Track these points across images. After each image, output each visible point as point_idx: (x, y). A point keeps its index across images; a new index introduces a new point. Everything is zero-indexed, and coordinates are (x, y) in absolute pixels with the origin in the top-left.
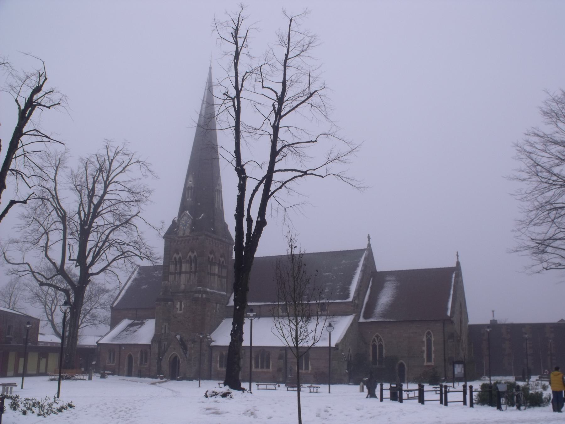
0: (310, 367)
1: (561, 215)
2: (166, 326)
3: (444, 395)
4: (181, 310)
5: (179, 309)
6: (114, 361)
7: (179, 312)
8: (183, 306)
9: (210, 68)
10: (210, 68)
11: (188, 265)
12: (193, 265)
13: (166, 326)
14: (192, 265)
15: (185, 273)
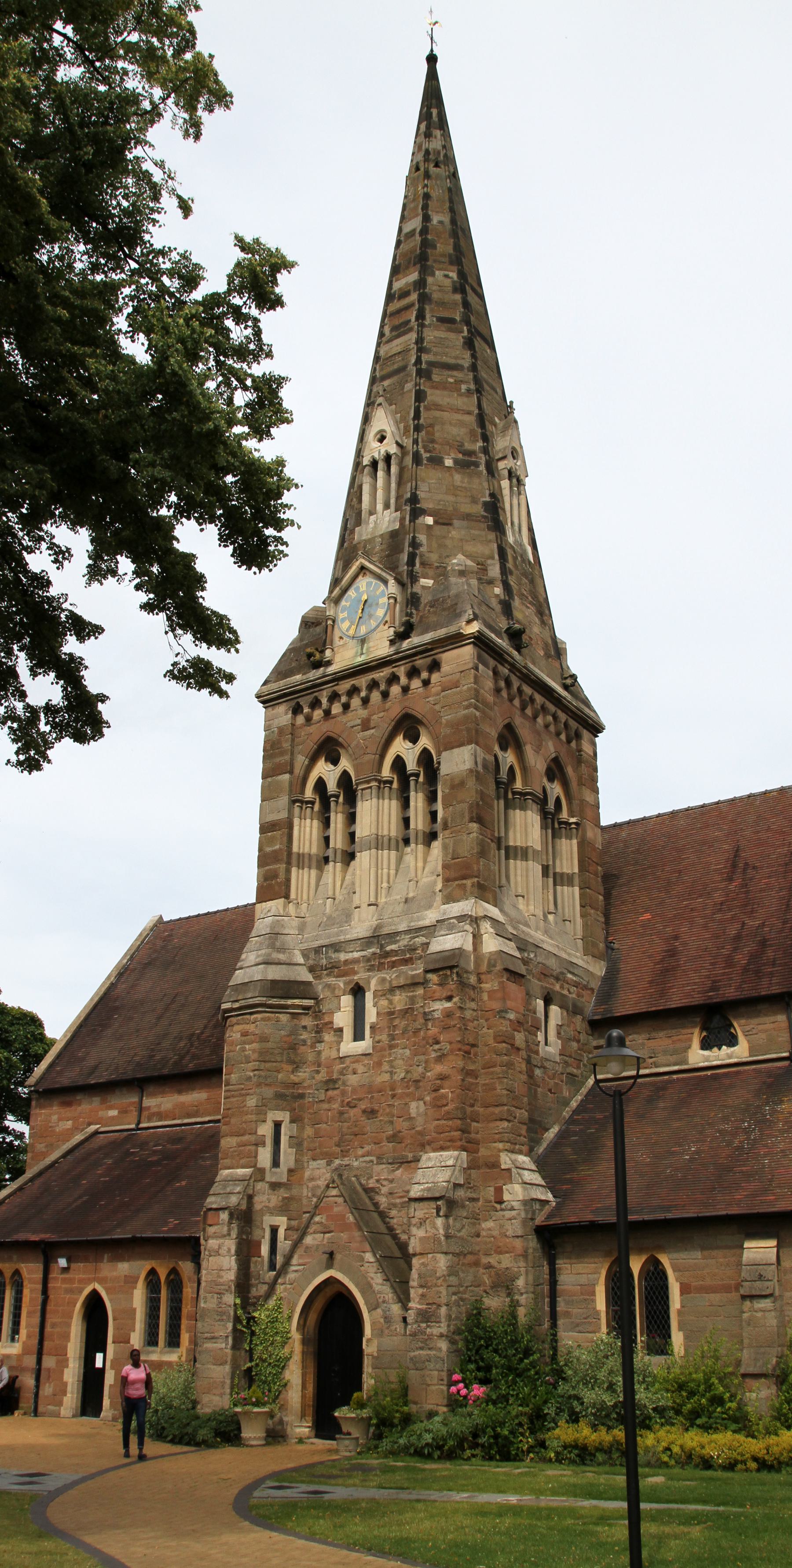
0: (677, 1338)
1: (525, 1189)
2: (277, 1125)
3: (164, 1294)
4: (358, 1035)
5: (348, 1033)
6: (15, 1331)
7: (349, 1047)
8: (371, 1015)
9: (432, 59)
10: (432, 59)
11: (391, 807)
12: (417, 800)
13: (277, 1125)
14: (412, 803)
15: (378, 843)
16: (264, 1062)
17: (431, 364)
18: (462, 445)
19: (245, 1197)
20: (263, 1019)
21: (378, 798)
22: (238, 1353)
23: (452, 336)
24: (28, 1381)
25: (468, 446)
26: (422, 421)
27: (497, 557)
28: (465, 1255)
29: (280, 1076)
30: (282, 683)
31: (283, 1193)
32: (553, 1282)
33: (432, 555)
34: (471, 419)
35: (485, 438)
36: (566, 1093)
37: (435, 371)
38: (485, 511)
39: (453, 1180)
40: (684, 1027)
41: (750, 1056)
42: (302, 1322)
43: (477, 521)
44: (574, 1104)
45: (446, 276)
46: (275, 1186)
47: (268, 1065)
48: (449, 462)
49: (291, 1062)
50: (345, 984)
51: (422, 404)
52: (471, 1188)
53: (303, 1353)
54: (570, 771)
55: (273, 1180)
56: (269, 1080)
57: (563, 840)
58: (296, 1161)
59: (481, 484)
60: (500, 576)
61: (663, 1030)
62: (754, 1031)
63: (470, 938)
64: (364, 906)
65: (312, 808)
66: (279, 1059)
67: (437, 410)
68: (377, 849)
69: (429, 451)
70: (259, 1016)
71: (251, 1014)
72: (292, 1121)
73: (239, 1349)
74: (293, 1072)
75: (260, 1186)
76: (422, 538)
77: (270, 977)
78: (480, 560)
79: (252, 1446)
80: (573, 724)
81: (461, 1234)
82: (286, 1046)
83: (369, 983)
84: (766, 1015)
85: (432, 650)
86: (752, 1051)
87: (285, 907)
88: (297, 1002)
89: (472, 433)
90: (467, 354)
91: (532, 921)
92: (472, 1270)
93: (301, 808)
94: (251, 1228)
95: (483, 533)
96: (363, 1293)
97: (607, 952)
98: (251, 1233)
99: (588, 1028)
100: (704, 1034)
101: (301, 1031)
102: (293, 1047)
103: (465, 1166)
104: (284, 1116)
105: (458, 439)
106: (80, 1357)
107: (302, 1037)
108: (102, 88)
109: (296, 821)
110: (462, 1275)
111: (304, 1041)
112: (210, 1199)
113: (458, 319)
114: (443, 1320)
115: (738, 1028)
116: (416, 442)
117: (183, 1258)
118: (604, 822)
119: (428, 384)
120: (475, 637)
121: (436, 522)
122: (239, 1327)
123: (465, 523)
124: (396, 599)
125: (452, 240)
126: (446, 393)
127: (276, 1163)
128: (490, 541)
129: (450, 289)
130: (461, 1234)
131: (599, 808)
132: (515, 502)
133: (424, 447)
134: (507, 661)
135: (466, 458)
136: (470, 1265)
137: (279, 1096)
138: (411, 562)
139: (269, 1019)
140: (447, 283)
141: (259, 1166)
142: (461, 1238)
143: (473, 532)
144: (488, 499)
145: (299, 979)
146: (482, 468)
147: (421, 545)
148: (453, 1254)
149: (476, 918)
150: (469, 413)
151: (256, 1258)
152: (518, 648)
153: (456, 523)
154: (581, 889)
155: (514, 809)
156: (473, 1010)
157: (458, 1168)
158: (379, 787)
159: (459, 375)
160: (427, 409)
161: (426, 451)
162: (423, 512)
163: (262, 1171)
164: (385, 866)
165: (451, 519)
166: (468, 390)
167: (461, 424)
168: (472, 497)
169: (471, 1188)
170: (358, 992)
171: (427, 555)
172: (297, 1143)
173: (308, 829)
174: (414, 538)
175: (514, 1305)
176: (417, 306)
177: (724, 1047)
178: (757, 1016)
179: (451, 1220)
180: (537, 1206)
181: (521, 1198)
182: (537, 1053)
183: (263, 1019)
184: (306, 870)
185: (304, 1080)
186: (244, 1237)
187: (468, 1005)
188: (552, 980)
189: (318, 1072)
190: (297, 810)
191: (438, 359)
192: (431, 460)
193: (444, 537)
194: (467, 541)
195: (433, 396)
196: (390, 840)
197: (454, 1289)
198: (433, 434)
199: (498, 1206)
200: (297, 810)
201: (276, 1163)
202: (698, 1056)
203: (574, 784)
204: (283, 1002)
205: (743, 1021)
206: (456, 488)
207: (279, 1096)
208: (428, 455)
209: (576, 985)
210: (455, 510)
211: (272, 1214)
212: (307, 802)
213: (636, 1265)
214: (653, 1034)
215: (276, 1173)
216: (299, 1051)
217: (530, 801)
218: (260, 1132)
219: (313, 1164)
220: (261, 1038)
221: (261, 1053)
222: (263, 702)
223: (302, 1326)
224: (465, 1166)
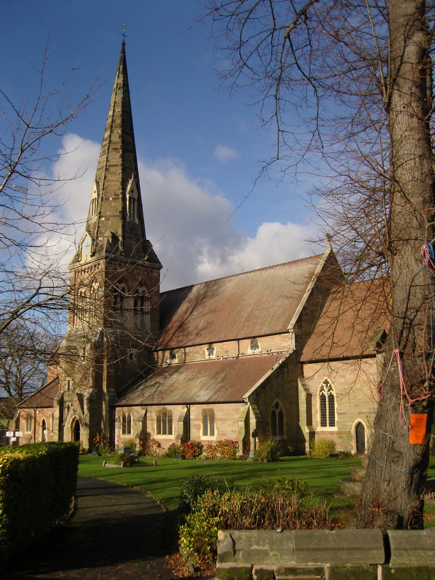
2: (69, 381)
9: (124, 44)
10: (124, 44)
13: (69, 381)
25: (117, 193)
37: (111, 168)
45: (117, 132)
48: (111, 199)
80: (150, 269)
108: (410, 187)
118: (160, 292)
121: (105, 219)
132: (132, 207)
144: (121, 209)
160: (107, 182)
162: (102, 217)
176: (108, 145)
192: (106, 199)
195: (109, 177)
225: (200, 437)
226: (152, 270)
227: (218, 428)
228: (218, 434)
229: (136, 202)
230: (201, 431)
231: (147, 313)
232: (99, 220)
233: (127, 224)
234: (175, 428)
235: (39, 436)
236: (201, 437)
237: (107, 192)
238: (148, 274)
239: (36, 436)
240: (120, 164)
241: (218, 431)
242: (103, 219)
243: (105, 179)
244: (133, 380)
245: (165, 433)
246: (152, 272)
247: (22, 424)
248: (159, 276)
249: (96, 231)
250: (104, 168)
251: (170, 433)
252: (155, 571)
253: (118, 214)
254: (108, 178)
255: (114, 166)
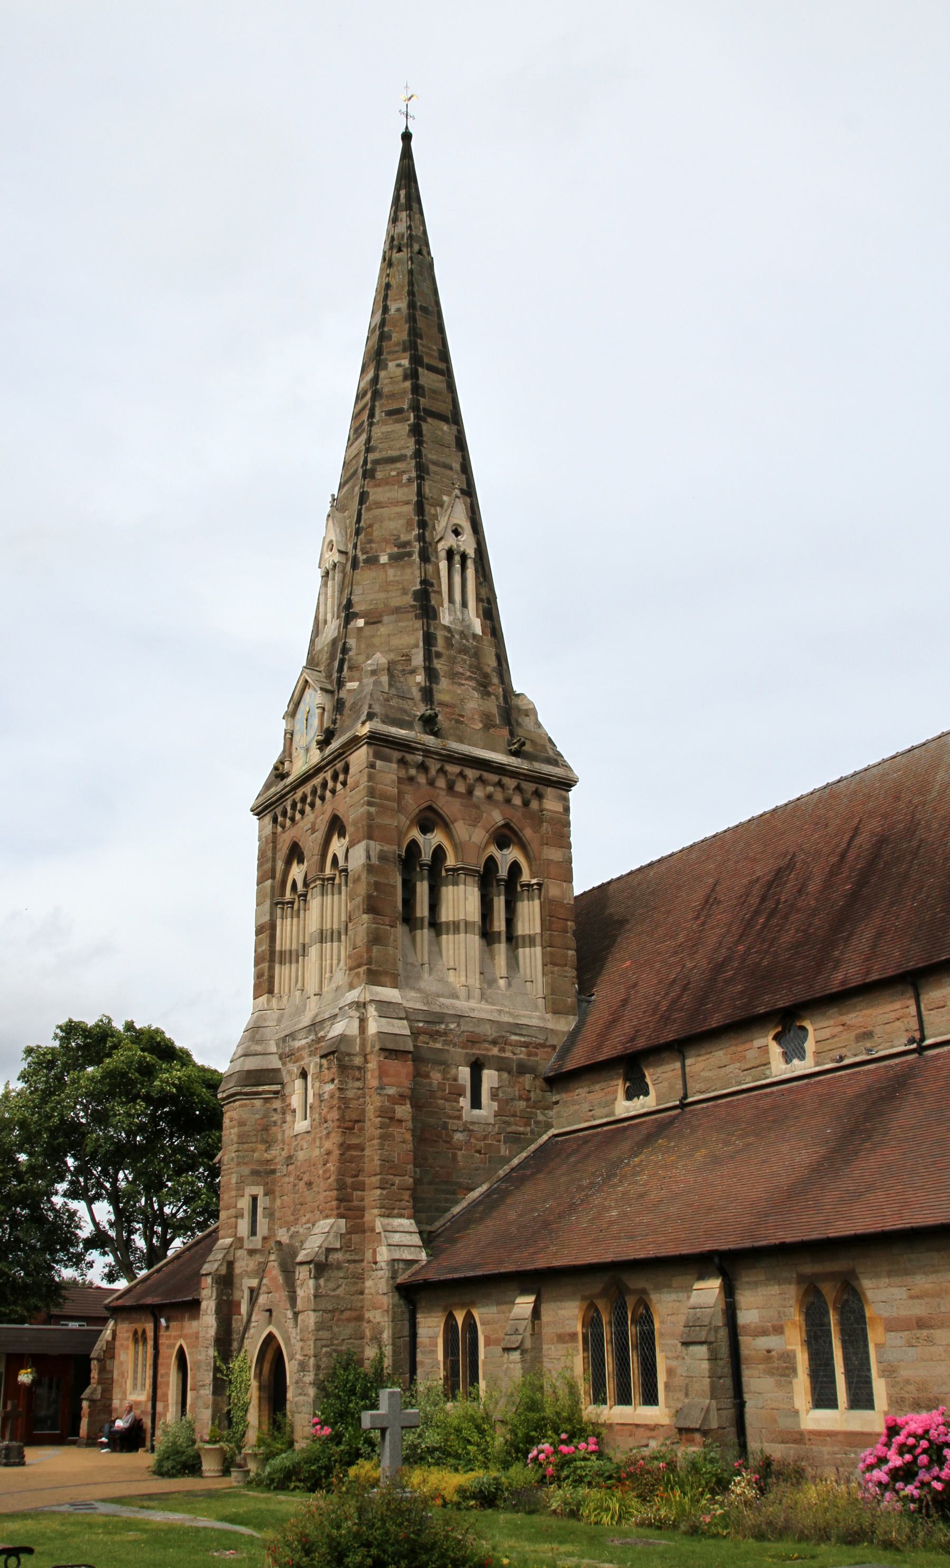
1: (390, 1251)
2: (254, 1199)
9: (407, 137)
10: (407, 137)
13: (254, 1199)
16: (243, 1143)
17: (376, 462)
18: (399, 537)
19: (225, 1264)
20: (241, 1106)
21: (323, 895)
22: (219, 1398)
23: (398, 427)
24: (147, 1422)
25: (404, 538)
26: (362, 524)
27: (421, 644)
28: (342, 1312)
29: (255, 1155)
30: (265, 796)
31: (259, 1258)
32: (413, 1335)
33: (360, 656)
34: (409, 509)
35: (423, 525)
36: (504, 1151)
37: (379, 468)
38: (415, 600)
39: (325, 1245)
40: (612, 1079)
41: (657, 1105)
42: (258, 1372)
43: (405, 612)
44: (515, 1161)
45: (399, 365)
46: (252, 1252)
47: (245, 1146)
48: (384, 559)
49: (264, 1141)
50: (298, 1069)
51: (364, 506)
52: (351, 1251)
53: (260, 1398)
54: (528, 833)
55: (250, 1247)
56: (246, 1160)
57: (526, 902)
58: (269, 1229)
59: (413, 573)
60: (422, 663)
61: (598, 1083)
62: (660, 1080)
63: (356, 1023)
64: (312, 996)
65: (292, 908)
66: (254, 1140)
67: (377, 508)
68: (322, 942)
69: (366, 553)
70: (237, 1103)
71: (234, 1101)
72: (266, 1194)
73: (220, 1395)
74: (266, 1151)
75: (239, 1253)
76: (352, 642)
77: (246, 1068)
78: (404, 651)
79: (207, 1477)
81: (337, 1292)
82: (260, 1128)
83: (309, 1067)
84: (668, 1063)
85: (344, 753)
86: (659, 1099)
87: (269, 1001)
88: (266, 1088)
89: (409, 523)
90: (412, 441)
91: (462, 992)
92: (353, 1324)
93: (283, 909)
94: (232, 1289)
95: (411, 623)
96: (286, 1345)
97: (579, 1006)
98: (232, 1294)
99: (544, 1085)
100: (628, 1084)
101: (272, 1113)
102: (266, 1129)
103: (344, 1231)
104: (258, 1190)
105: (395, 532)
106: (177, 1403)
107: (273, 1119)
109: (279, 922)
110: (336, 1329)
111: (275, 1122)
112: (206, 1266)
113: (406, 407)
114: (311, 1369)
115: (650, 1076)
116: (355, 547)
117: (146, 1321)
119: (371, 484)
120: (368, 738)
121: (366, 623)
122: (219, 1375)
123: (393, 617)
124: (324, 709)
125: (407, 325)
126: (387, 488)
127: (253, 1232)
128: (417, 630)
129: (401, 378)
130: (337, 1292)
131: (571, 863)
132: (457, 579)
133: (362, 550)
134: (418, 749)
135: (402, 550)
136: (349, 1320)
137: (255, 1173)
138: (340, 670)
139: (246, 1105)
140: (399, 372)
141: (238, 1235)
142: (338, 1297)
143: (400, 624)
144: (418, 587)
145: (270, 1067)
146: (416, 557)
147: (350, 650)
148: (324, 1311)
149: (364, 1004)
150: (407, 503)
151: (237, 1316)
152: (436, 734)
153: (386, 619)
154: (543, 947)
155: (447, 886)
156: (359, 1089)
157: (332, 1234)
158: (323, 885)
159: (400, 466)
161: (363, 553)
162: (356, 616)
163: (241, 1240)
164: (328, 957)
165: (381, 616)
166: (409, 480)
167: (399, 515)
168: (403, 589)
169: (351, 1251)
170: (304, 1075)
171: (355, 658)
172: (270, 1214)
173: (289, 928)
174: (345, 643)
175: (382, 1355)
177: (641, 1097)
178: (661, 1065)
179: (322, 1281)
180: (401, 1265)
181: (386, 1259)
182: (459, 1118)
183: (241, 1106)
184: (287, 965)
185: (275, 1157)
186: (225, 1298)
187: (350, 1085)
188: (486, 1045)
189: (283, 1149)
190: (279, 911)
191: (384, 454)
192: (367, 561)
193: (373, 636)
194: (395, 635)
195: (376, 494)
196: (332, 933)
197: (324, 1342)
198: (371, 535)
199: (374, 1266)
200: (279, 911)
201: (253, 1232)
202: (624, 1107)
203: (534, 846)
204: (255, 1089)
205: (652, 1070)
206: (388, 583)
207: (255, 1173)
208: (365, 557)
209: (526, 1045)
210: (386, 605)
211: (249, 1277)
212: (288, 903)
213: (460, 1317)
214: (593, 1088)
215: (252, 1241)
216: (271, 1132)
217: (463, 876)
218: (239, 1206)
219: (280, 1231)
220: (239, 1123)
221: (239, 1136)
222: (257, 814)
223: (259, 1375)
224: (344, 1231)
225: (796, 1413)
226: (541, 787)
227: (889, 1372)
228: (896, 1402)
229: (470, 564)
230: (802, 1383)
231: (530, 941)
232: (345, 627)
233: (440, 635)
234: (670, 1372)
235: (166, 1407)
236: (802, 1415)
237: (371, 541)
238: (526, 804)
239: (160, 1407)
240: (409, 452)
241: (891, 1386)
242: (361, 622)
243: (361, 502)
244: (485, 1187)
245: (624, 1398)
246: (539, 795)
247: (121, 1363)
248: (567, 810)
249: (336, 664)
250: (360, 471)
251: (650, 1398)
252: (61, 1140)
253: (409, 600)
254: (372, 498)
255: (392, 460)
